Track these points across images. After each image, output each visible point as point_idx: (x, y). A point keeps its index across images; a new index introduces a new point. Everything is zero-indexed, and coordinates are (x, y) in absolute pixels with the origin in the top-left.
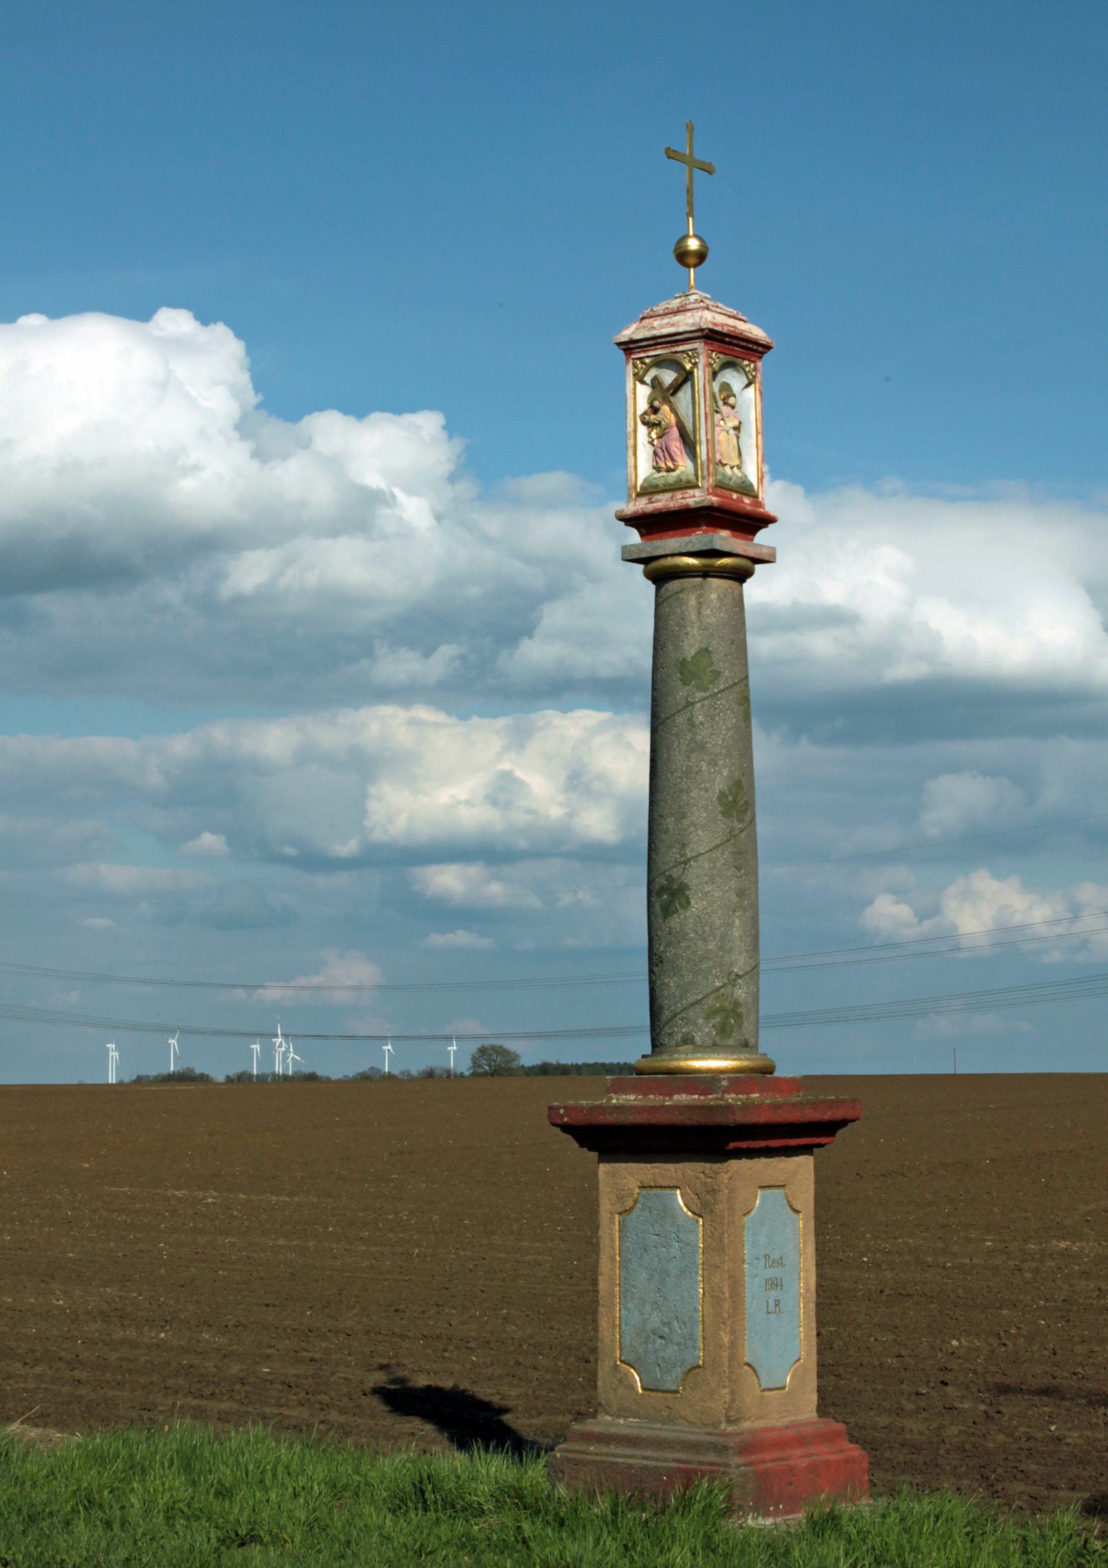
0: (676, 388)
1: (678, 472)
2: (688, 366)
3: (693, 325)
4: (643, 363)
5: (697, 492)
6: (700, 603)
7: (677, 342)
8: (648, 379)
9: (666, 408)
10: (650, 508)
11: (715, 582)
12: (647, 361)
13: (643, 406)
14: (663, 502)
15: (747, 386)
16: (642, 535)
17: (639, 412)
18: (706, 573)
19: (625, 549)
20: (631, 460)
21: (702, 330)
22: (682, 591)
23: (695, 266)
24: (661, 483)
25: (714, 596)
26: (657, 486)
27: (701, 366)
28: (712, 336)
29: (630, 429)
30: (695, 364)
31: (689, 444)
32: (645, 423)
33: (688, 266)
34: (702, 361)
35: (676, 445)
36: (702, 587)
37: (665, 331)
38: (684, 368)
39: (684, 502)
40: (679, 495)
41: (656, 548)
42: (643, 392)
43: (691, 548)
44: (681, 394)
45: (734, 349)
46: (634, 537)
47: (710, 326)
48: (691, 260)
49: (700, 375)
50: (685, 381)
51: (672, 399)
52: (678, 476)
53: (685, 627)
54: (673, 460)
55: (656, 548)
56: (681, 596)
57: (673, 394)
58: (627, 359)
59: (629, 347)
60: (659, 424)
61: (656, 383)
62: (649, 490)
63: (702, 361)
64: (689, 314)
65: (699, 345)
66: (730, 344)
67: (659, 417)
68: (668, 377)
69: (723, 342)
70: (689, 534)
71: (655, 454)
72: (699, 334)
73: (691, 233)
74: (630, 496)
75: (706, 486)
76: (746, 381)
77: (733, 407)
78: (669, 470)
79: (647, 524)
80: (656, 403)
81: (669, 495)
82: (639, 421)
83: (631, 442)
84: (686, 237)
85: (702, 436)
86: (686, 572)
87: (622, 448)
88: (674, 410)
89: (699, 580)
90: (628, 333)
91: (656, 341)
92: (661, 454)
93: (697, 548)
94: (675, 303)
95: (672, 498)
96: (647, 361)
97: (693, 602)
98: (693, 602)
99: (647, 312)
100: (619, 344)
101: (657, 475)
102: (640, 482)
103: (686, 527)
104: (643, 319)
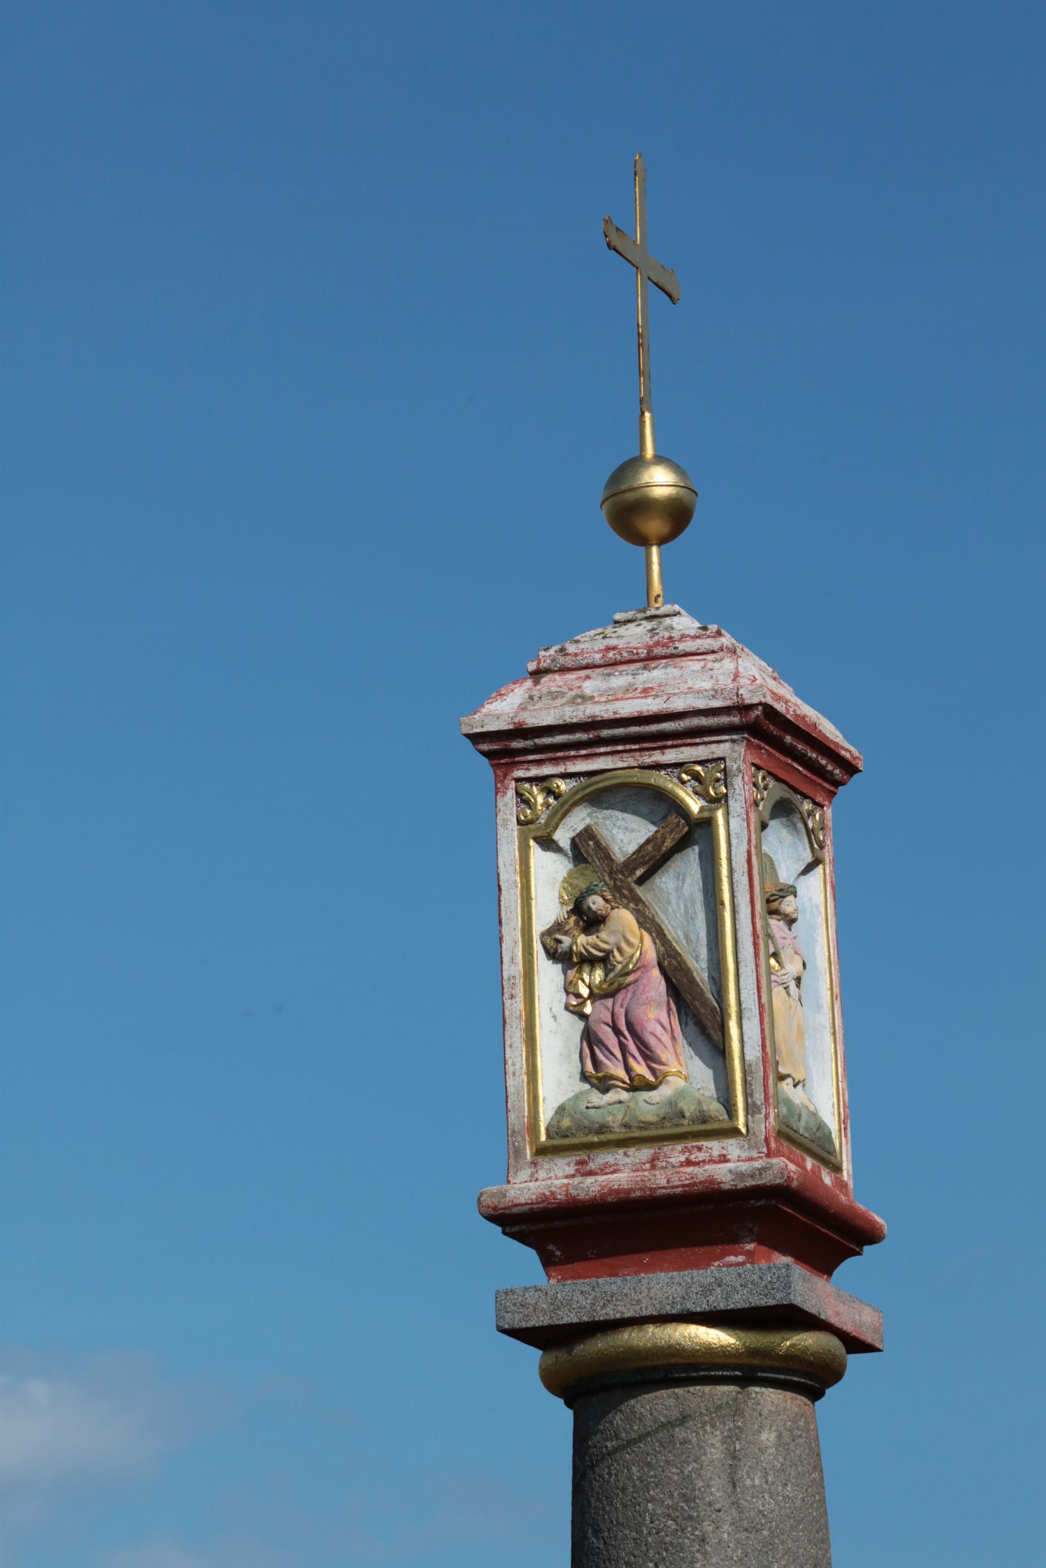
0: (652, 861)
1: (664, 1092)
2: (695, 805)
3: (716, 693)
4: (549, 792)
5: (732, 1148)
6: (734, 1455)
7: (662, 740)
8: (563, 836)
9: (624, 917)
10: (591, 1187)
11: (769, 1398)
12: (563, 786)
13: (548, 908)
14: (623, 1173)
15: (809, 869)
16: (548, 1262)
17: (539, 925)
18: (745, 1372)
19: (503, 1297)
20: (516, 1055)
21: (744, 708)
22: (683, 1420)
23: (662, 541)
24: (615, 1118)
25: (767, 1437)
26: (602, 1129)
27: (737, 805)
28: (764, 727)
29: (513, 969)
30: (720, 800)
31: (701, 1016)
32: (553, 955)
33: (643, 541)
34: (741, 791)
35: (656, 1015)
36: (738, 1412)
37: (628, 708)
38: (681, 809)
39: (700, 1173)
40: (675, 1154)
41: (610, 1299)
42: (550, 872)
43: (718, 1301)
44: (665, 881)
45: (799, 762)
46: (522, 1264)
47: (769, 700)
48: (655, 526)
49: (731, 830)
50: (682, 845)
51: (640, 891)
52: (671, 1103)
53: (697, 1521)
54: (648, 1056)
55: (610, 1299)
56: (680, 1433)
57: (641, 881)
58: (500, 780)
59: (505, 749)
60: (605, 960)
61: (585, 850)
62: (574, 1139)
63: (741, 791)
64: (694, 665)
65: (733, 752)
66: (789, 752)
67: (604, 938)
68: (626, 834)
69: (777, 744)
70: (703, 1263)
71: (590, 1038)
72: (736, 719)
73: (650, 452)
74: (518, 1153)
75: (761, 1130)
76: (808, 858)
77: (791, 921)
78: (636, 1085)
79: (561, 1232)
80: (596, 903)
81: (644, 1153)
82: (537, 947)
83: (515, 1007)
84: (637, 462)
85: (741, 992)
86: (696, 1367)
87: (489, 1021)
88: (647, 922)
89: (731, 1389)
90: (503, 709)
91: (594, 734)
92: (611, 1041)
93: (739, 1301)
94: (635, 636)
95: (653, 1162)
96: (563, 786)
97: (715, 1452)
98: (715, 1452)
99: (546, 657)
100: (476, 738)
101: (597, 1098)
102: (545, 1115)
103: (602, 1254)
104: (537, 674)
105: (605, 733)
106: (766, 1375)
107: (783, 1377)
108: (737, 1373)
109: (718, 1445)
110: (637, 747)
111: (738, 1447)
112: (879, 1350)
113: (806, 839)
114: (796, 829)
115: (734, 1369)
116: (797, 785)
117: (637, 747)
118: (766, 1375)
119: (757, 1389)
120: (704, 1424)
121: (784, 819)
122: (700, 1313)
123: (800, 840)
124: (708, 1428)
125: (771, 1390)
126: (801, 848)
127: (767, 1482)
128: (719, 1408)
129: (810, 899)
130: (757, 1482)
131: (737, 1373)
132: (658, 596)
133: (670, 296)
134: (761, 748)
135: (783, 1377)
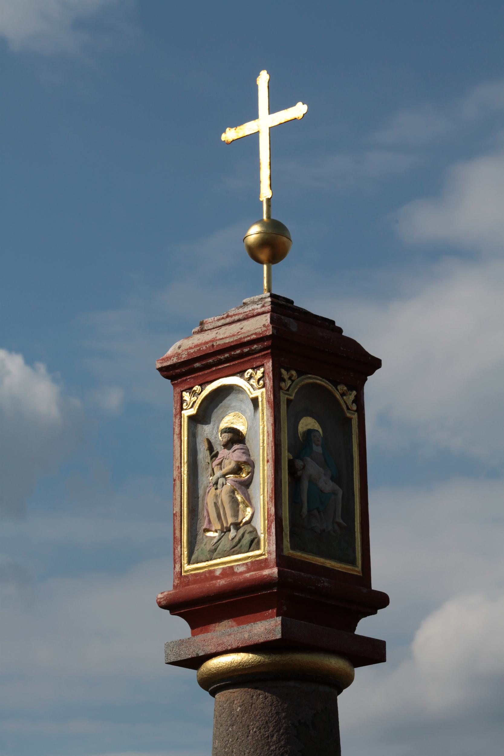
134: (186, 379)
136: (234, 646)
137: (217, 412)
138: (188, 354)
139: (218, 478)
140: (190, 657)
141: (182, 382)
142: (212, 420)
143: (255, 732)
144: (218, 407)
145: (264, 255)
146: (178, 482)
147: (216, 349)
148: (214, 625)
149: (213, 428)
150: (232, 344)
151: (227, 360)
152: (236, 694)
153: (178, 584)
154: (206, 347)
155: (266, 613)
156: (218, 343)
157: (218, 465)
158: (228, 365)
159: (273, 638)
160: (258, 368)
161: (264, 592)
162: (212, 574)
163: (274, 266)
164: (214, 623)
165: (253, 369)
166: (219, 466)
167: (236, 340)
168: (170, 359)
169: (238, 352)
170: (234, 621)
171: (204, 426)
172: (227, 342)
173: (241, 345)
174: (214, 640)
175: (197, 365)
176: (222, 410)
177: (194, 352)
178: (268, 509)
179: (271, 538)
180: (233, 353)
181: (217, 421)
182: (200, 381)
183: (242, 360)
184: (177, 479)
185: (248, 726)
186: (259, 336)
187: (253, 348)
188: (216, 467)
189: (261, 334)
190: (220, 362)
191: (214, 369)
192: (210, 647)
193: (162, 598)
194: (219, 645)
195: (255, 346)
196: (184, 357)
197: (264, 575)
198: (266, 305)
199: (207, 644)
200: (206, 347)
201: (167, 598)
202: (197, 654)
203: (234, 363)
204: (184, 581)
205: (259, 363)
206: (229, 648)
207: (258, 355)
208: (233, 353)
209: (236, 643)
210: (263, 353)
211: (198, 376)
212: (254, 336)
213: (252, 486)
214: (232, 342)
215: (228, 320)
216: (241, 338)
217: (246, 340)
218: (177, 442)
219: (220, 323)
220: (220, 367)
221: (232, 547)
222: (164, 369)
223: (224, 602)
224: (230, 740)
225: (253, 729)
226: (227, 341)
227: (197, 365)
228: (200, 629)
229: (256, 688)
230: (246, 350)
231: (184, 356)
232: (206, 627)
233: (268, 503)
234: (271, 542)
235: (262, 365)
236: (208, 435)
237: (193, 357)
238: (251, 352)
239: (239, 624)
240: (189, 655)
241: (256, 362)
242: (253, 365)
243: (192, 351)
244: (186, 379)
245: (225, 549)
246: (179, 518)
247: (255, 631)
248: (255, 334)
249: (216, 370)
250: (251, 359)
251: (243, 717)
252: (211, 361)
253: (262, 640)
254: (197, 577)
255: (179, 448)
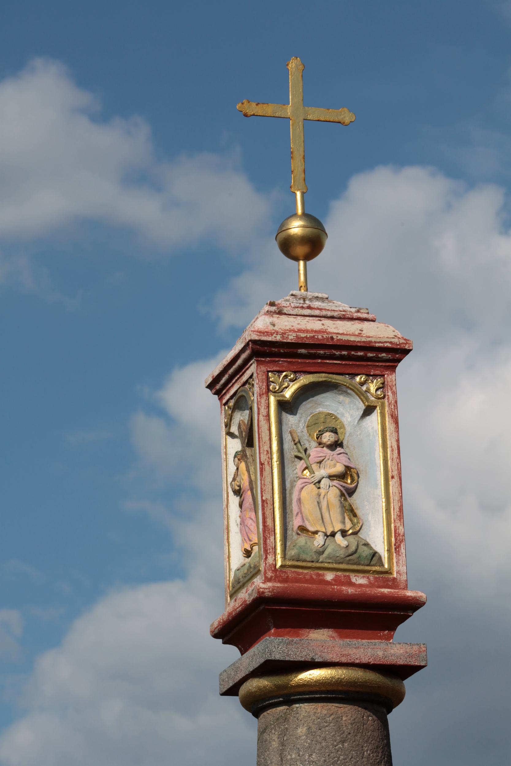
6: (283, 744)
25: (301, 731)
36: (286, 720)
105: (231, 371)
106: (296, 697)
107: (308, 696)
108: (281, 699)
109: (276, 739)
110: (238, 376)
111: (285, 739)
112: (418, 668)
113: (358, 397)
114: (346, 392)
115: (279, 698)
116: (339, 371)
117: (238, 376)
118: (296, 697)
119: (297, 705)
120: (271, 729)
121: (335, 391)
122: (357, 664)
123: (354, 398)
124: (273, 731)
125: (306, 704)
126: (357, 403)
127: (299, 755)
128: (278, 719)
129: (373, 428)
130: (293, 756)
131: (281, 699)
132: (301, 287)
133: (339, 122)
134: (279, 361)
135: (308, 696)
136: (365, 660)
137: (305, 405)
138: (296, 336)
139: (323, 477)
140: (303, 659)
141: (270, 362)
142: (298, 412)
143: (369, 755)
144: (308, 401)
145: (300, 250)
146: (267, 468)
147: (335, 342)
148: (308, 630)
149: (299, 421)
150: (359, 344)
151: (341, 358)
152: (346, 709)
153: (272, 577)
154: (323, 337)
155: (380, 633)
156: (340, 337)
157: (318, 463)
158: (339, 362)
159: (416, 664)
160: (375, 376)
161: (396, 613)
162: (321, 578)
163: (308, 263)
164: (308, 628)
165: (368, 375)
166: (318, 465)
167: (364, 342)
168: (272, 335)
169: (360, 354)
170: (337, 632)
171: (288, 415)
172: (352, 340)
173: (368, 347)
174: (337, 649)
175: (303, 351)
176: (311, 405)
177: (306, 337)
178: (395, 527)
179: (400, 558)
180: (353, 353)
181: (304, 415)
182: (295, 368)
183: (358, 363)
184: (266, 463)
185: (362, 747)
186: (395, 347)
187: (380, 356)
188: (316, 464)
189: (397, 345)
190: (333, 357)
191: (320, 361)
192: (331, 656)
193: (266, 589)
194: (343, 655)
195: (384, 355)
196: (291, 338)
197: (409, 597)
198: (362, 311)
199: (326, 650)
200: (323, 337)
201: (273, 590)
202: (312, 658)
203: (347, 363)
204: (280, 576)
205: (378, 372)
206: (357, 661)
207: (381, 364)
208: (353, 353)
209: (367, 659)
210: (388, 364)
211: (295, 362)
212: (389, 345)
213: (355, 496)
214: (358, 342)
215: (307, 312)
216: (371, 342)
217: (377, 345)
218: (377, 438)
219: (295, 311)
220: (328, 361)
221: (347, 554)
222: (259, 343)
223: (342, 610)
224: (342, 757)
225: (367, 751)
226: (352, 339)
227: (303, 351)
228: (287, 630)
229: (366, 709)
230: (370, 355)
231: (291, 337)
232: (296, 630)
233: (395, 521)
234: (401, 562)
235: (383, 376)
236: (294, 426)
237: (304, 342)
238: (374, 358)
239: (342, 637)
240: (302, 657)
241: (375, 370)
242: (370, 372)
243: (303, 335)
244: (279, 361)
245: (338, 555)
246: (270, 507)
247: (392, 651)
248: (391, 343)
249: (321, 363)
250: (371, 365)
251: (356, 736)
252: (322, 352)
253: (401, 662)
254: (299, 575)
255: (268, 432)
